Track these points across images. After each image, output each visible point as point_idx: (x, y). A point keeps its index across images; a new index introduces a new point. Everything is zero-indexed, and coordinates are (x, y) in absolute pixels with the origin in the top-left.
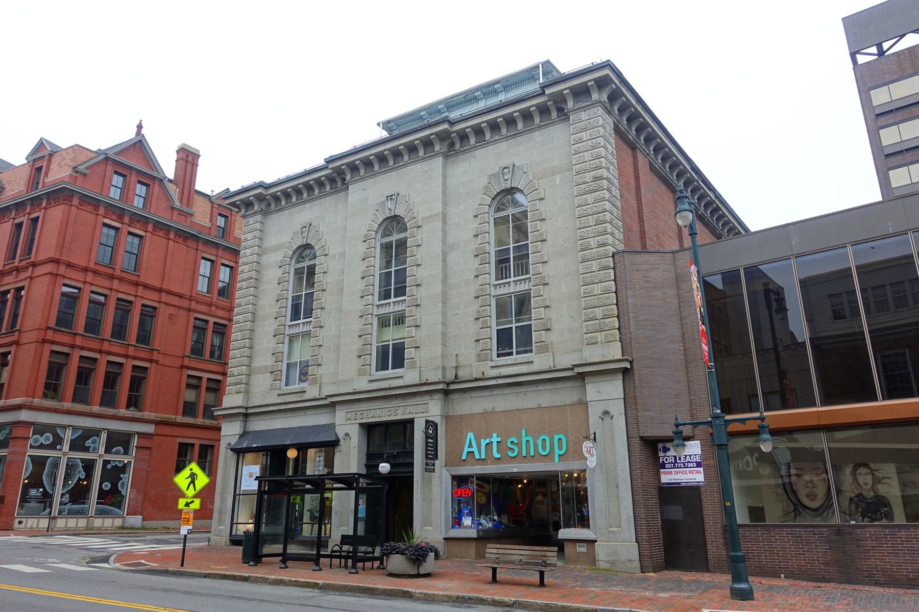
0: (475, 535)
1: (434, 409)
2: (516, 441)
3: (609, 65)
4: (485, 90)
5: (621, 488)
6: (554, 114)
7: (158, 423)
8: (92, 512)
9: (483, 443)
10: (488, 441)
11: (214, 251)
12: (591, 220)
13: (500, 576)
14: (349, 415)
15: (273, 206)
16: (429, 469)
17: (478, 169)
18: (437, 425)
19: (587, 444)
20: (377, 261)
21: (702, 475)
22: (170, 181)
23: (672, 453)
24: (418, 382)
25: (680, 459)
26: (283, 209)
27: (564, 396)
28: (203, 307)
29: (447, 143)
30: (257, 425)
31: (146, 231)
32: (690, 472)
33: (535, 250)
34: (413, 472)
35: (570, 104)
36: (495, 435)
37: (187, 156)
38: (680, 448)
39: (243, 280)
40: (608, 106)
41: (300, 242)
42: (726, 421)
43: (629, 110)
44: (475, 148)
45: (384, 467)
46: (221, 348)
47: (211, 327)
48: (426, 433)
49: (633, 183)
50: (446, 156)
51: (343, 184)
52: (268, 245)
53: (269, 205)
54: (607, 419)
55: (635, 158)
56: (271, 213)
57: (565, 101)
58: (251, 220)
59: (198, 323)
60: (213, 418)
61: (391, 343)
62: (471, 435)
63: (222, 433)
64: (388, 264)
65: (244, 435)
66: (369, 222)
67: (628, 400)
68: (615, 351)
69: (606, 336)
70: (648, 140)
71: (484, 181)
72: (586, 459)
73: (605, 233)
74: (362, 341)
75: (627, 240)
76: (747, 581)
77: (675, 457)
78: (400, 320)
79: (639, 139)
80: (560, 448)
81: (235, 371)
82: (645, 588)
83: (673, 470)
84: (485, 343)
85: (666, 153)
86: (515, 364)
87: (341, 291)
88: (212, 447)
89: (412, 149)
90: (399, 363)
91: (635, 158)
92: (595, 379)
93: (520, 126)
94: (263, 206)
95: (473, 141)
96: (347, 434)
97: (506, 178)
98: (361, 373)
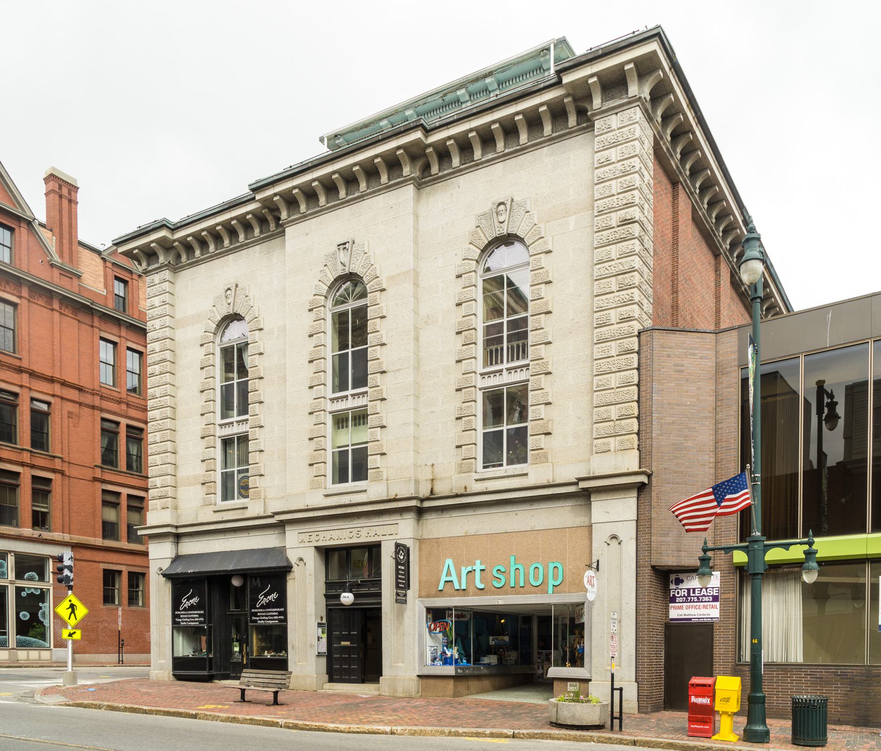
0: (453, 673)
1: (404, 529)
2: (503, 570)
3: (658, 35)
4: (473, 87)
5: (624, 623)
6: (572, 120)
7: (75, 546)
8: (12, 643)
9: (464, 571)
10: (469, 569)
11: (115, 330)
12: (613, 284)
13: (248, 696)
14: (303, 537)
15: (184, 258)
16: (401, 599)
17: (468, 198)
18: (408, 550)
19: (590, 573)
20: (329, 338)
21: (718, 610)
22: (41, 225)
23: (685, 585)
24: (385, 498)
25: (694, 592)
26: (197, 263)
27: (562, 516)
28: (110, 404)
29: (420, 164)
30: (189, 547)
31: (20, 297)
32: (704, 607)
33: (537, 325)
34: (380, 603)
35: (597, 102)
36: (478, 562)
37: (60, 187)
38: (706, 578)
39: (155, 364)
40: (649, 106)
41: (225, 311)
42: (765, 546)
43: (676, 118)
44: (458, 172)
45: (347, 598)
46: (139, 457)
47: (123, 431)
48: (396, 559)
49: (670, 235)
50: (420, 186)
51: (278, 225)
52: (183, 307)
53: (179, 256)
54: (614, 543)
55: (675, 197)
56: (183, 268)
57: (589, 97)
58: (157, 278)
59: (107, 425)
60: (139, 540)
61: (350, 448)
62: (449, 562)
63: (150, 557)
64: (343, 345)
65: (177, 559)
66: (317, 282)
67: (643, 524)
68: (630, 462)
69: (622, 442)
70: (695, 172)
71: (471, 224)
72: (586, 591)
73: (631, 302)
74: (313, 445)
75: (656, 316)
76: (764, 723)
77: (689, 590)
78: (361, 417)
79: (684, 168)
80: (555, 578)
81: (158, 481)
82: (648, 730)
83: (685, 604)
84: (468, 450)
85: (716, 194)
86: (506, 477)
87: (284, 379)
88: (144, 575)
89: (371, 171)
90: (361, 473)
91: (675, 197)
92: (604, 497)
93: (524, 138)
94: (171, 259)
95: (456, 161)
96: (301, 560)
97: (501, 219)
98: (314, 486)
